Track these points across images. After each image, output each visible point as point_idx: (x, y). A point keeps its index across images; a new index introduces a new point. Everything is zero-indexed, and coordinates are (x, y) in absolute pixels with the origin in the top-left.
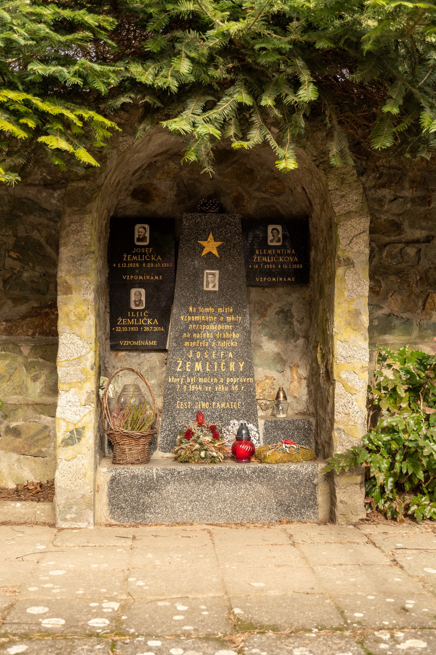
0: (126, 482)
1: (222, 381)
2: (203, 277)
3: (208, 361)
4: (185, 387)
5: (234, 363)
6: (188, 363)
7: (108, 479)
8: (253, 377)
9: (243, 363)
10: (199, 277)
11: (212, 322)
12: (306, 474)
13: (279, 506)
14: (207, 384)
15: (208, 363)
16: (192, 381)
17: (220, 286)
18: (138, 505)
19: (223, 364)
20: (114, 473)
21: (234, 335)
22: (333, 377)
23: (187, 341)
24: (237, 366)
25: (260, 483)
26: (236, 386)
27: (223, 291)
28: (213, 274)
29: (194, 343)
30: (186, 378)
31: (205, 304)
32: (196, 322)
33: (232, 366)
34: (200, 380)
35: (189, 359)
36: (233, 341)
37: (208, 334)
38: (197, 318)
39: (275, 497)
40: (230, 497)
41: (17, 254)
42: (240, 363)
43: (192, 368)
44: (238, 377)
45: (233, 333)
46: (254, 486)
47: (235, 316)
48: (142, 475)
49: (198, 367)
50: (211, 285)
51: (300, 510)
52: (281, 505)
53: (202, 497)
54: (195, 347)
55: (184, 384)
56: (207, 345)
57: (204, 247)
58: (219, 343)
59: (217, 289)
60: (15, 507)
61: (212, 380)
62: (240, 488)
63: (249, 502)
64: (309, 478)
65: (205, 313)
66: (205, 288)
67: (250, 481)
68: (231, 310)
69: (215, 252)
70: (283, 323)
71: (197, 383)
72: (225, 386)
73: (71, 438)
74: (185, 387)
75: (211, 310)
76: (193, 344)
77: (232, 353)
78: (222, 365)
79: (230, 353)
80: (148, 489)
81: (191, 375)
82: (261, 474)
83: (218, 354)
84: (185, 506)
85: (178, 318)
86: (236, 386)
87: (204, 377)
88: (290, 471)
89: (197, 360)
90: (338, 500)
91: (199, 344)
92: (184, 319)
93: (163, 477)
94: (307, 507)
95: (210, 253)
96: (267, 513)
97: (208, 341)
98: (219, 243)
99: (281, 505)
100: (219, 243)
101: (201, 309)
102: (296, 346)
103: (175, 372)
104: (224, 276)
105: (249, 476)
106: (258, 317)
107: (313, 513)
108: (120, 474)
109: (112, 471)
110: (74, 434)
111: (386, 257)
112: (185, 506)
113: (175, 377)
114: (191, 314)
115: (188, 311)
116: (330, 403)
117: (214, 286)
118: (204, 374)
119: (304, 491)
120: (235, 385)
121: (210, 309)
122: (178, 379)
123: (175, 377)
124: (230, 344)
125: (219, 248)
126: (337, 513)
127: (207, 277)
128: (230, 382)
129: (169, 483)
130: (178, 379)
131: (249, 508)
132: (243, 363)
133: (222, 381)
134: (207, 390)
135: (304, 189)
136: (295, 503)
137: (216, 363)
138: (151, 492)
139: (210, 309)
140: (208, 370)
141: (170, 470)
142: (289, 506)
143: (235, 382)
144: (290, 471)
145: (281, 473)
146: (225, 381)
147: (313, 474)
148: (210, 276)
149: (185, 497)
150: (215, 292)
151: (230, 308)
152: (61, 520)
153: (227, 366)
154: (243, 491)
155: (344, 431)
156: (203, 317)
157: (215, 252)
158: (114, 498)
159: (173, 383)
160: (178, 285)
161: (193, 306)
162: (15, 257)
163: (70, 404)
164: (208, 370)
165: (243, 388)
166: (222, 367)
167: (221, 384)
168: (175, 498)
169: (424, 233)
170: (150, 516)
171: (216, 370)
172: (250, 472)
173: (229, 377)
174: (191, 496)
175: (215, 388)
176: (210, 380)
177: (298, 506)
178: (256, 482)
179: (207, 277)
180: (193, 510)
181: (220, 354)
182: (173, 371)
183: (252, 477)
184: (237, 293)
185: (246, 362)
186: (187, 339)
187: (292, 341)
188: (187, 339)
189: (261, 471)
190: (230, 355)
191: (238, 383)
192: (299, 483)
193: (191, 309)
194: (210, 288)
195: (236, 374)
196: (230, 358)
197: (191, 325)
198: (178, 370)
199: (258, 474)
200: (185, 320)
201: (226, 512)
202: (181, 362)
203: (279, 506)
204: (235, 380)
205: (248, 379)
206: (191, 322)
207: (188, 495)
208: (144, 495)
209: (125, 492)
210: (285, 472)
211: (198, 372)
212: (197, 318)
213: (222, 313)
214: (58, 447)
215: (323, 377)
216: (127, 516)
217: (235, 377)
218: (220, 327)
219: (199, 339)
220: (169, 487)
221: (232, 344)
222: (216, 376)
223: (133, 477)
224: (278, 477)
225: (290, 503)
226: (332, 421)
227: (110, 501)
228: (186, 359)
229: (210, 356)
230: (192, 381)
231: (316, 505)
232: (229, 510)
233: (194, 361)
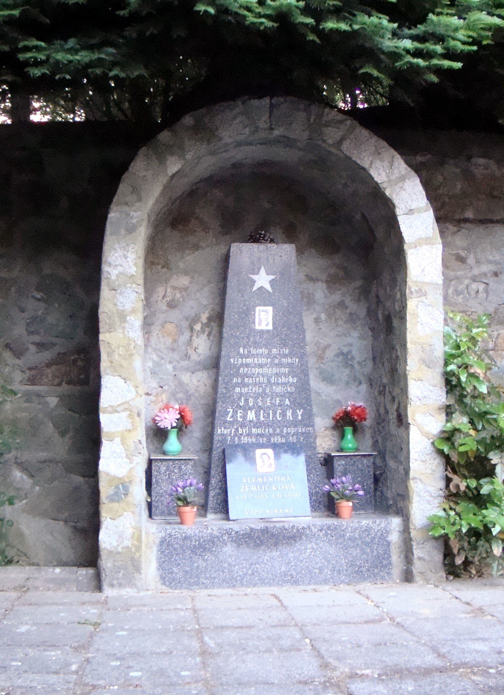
0: (177, 543)
1: (278, 431)
2: (254, 315)
3: (262, 409)
4: (236, 439)
5: (291, 411)
6: (239, 411)
7: (158, 541)
8: (313, 426)
9: (302, 410)
10: (250, 314)
11: (266, 365)
12: (379, 530)
13: (350, 567)
14: (262, 435)
15: (262, 412)
16: (244, 432)
17: (274, 324)
18: (192, 570)
19: (279, 411)
20: (163, 534)
21: (291, 379)
22: (407, 420)
23: (238, 387)
24: (294, 414)
25: (328, 543)
26: (295, 437)
27: (277, 330)
28: (266, 311)
29: (246, 389)
30: (237, 430)
31: (256, 345)
32: (247, 365)
33: (289, 414)
34: (254, 431)
35: (240, 406)
36: (290, 386)
37: (262, 379)
38: (249, 361)
39: (346, 557)
40: (294, 558)
41: (41, 294)
42: (298, 411)
43: (244, 417)
44: (296, 426)
45: (290, 377)
46: (321, 545)
47: (291, 358)
48: (195, 535)
49: (251, 415)
50: (264, 323)
51: (373, 571)
52: (352, 565)
53: (263, 560)
54: (247, 393)
55: (235, 435)
56: (261, 391)
57: (255, 282)
58: (274, 388)
59: (270, 327)
60: (53, 573)
61: (267, 430)
62: (306, 549)
63: (316, 564)
64: (382, 535)
65: (257, 355)
66: (257, 327)
67: (317, 540)
68: (287, 351)
69: (268, 287)
70: (343, 366)
71: (249, 435)
72: (282, 437)
73: (116, 494)
74: (236, 439)
75: (265, 351)
76: (245, 390)
77: (289, 400)
78: (278, 413)
79: (287, 400)
80: (202, 552)
81: (243, 426)
82: (329, 532)
83: (273, 401)
84: (244, 570)
85: (228, 360)
86: (295, 437)
87: (258, 428)
88: (361, 528)
89: (250, 409)
90: (415, 556)
91: (252, 390)
92: (234, 361)
93: (219, 538)
94: (381, 567)
95: (261, 288)
96: (336, 574)
97: (261, 386)
98: (272, 277)
99: (352, 565)
100: (272, 277)
101: (253, 351)
102: (358, 392)
103: (225, 422)
104: (279, 313)
105: (314, 535)
106: (315, 360)
107: (388, 573)
108: (170, 535)
109: (161, 532)
110: (119, 489)
111: (453, 294)
112: (244, 570)
113: (225, 428)
114: (242, 356)
115: (239, 353)
116: (404, 451)
117: (267, 324)
118: (258, 424)
119: (376, 550)
120: (293, 436)
121: (263, 349)
122: (229, 430)
123: (225, 428)
124: (286, 390)
125: (272, 282)
126: (415, 571)
127: (259, 315)
128: (287, 433)
129: (226, 544)
130: (229, 430)
131: (316, 570)
132: (302, 410)
133: (278, 431)
134: (261, 442)
135: (363, 216)
136: (367, 563)
137: (271, 412)
138: (206, 555)
139: (263, 349)
140: (262, 419)
141: (226, 530)
142: (360, 567)
143: (293, 432)
144: (361, 528)
145: (351, 529)
146: (282, 431)
147: (386, 531)
148: (262, 313)
149: (245, 560)
150: (268, 331)
151: (286, 349)
152: (108, 586)
153: (284, 414)
154: (309, 551)
155: (421, 480)
156: (256, 359)
157: (268, 287)
158: (164, 562)
159: (223, 435)
160: (227, 323)
161: (244, 347)
162: (39, 296)
163: (115, 455)
164: (262, 419)
165: (302, 438)
166: (278, 416)
167: (278, 435)
168: (233, 561)
169: (493, 268)
170: (205, 582)
171: (271, 419)
172: (316, 530)
173: (286, 426)
174: (250, 558)
175: (270, 439)
176: (264, 431)
177: (371, 567)
178: (323, 541)
179: (259, 315)
180: (253, 574)
181: (276, 400)
182: (223, 420)
183: (318, 535)
184: (293, 332)
185: (305, 409)
186: (237, 385)
187: (353, 387)
188: (237, 385)
189: (329, 528)
190: (287, 402)
191: (296, 434)
192: (372, 541)
193: (241, 350)
194: (263, 327)
195: (295, 423)
196: (287, 405)
197: (242, 369)
198: (228, 419)
199: (326, 532)
200: (236, 363)
201: (291, 575)
202: (231, 410)
203: (350, 567)
204: (292, 430)
205: (308, 429)
206: (242, 365)
207: (247, 558)
208: (198, 558)
209: (177, 554)
210: (356, 529)
211: (250, 421)
212: (249, 361)
213: (277, 354)
214: (128, 484)
215: (393, 423)
216: (179, 582)
217: (293, 427)
218: (275, 370)
219: (251, 384)
220: (226, 549)
221: (289, 389)
222: (271, 426)
223: (186, 538)
224: (348, 535)
225: (361, 563)
226: (407, 471)
227: (160, 566)
228: (237, 407)
229: (264, 403)
230: (244, 432)
231: (390, 564)
232: (294, 573)
233: (246, 408)
